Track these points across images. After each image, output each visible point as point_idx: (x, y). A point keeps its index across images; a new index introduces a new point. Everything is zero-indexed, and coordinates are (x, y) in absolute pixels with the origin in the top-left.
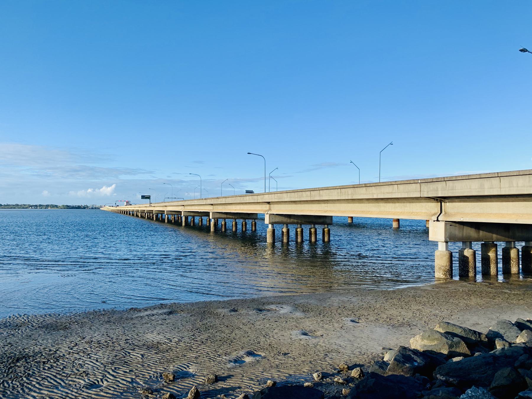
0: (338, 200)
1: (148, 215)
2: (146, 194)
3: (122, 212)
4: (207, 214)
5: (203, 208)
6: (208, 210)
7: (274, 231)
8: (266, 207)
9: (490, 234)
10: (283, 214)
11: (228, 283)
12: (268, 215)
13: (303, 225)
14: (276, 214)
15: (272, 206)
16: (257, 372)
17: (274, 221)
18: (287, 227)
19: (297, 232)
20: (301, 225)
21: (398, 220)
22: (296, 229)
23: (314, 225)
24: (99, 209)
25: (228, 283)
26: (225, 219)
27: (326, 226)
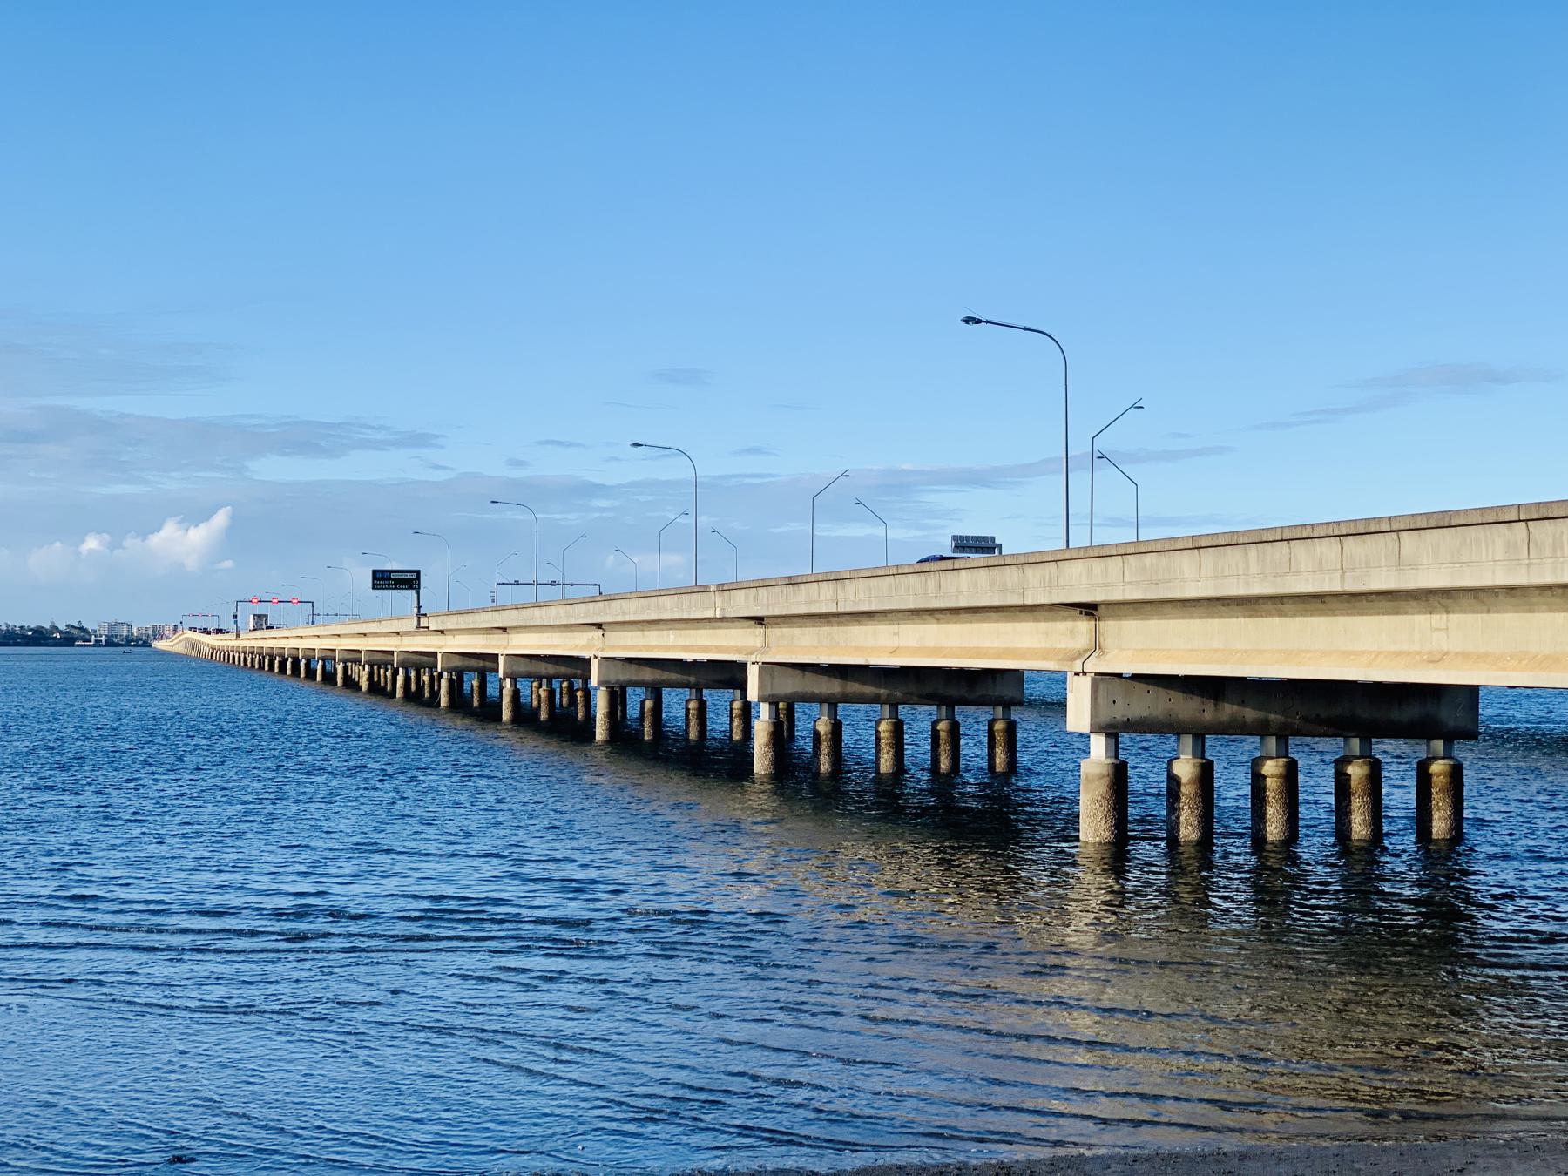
4: (730, 674)
6: (739, 650)
7: (1119, 775)
9: (685, 677)
10: (817, 665)
15: (1109, 626)
23: (1449, 741)
24: (146, 644)
27: (1438, 745)
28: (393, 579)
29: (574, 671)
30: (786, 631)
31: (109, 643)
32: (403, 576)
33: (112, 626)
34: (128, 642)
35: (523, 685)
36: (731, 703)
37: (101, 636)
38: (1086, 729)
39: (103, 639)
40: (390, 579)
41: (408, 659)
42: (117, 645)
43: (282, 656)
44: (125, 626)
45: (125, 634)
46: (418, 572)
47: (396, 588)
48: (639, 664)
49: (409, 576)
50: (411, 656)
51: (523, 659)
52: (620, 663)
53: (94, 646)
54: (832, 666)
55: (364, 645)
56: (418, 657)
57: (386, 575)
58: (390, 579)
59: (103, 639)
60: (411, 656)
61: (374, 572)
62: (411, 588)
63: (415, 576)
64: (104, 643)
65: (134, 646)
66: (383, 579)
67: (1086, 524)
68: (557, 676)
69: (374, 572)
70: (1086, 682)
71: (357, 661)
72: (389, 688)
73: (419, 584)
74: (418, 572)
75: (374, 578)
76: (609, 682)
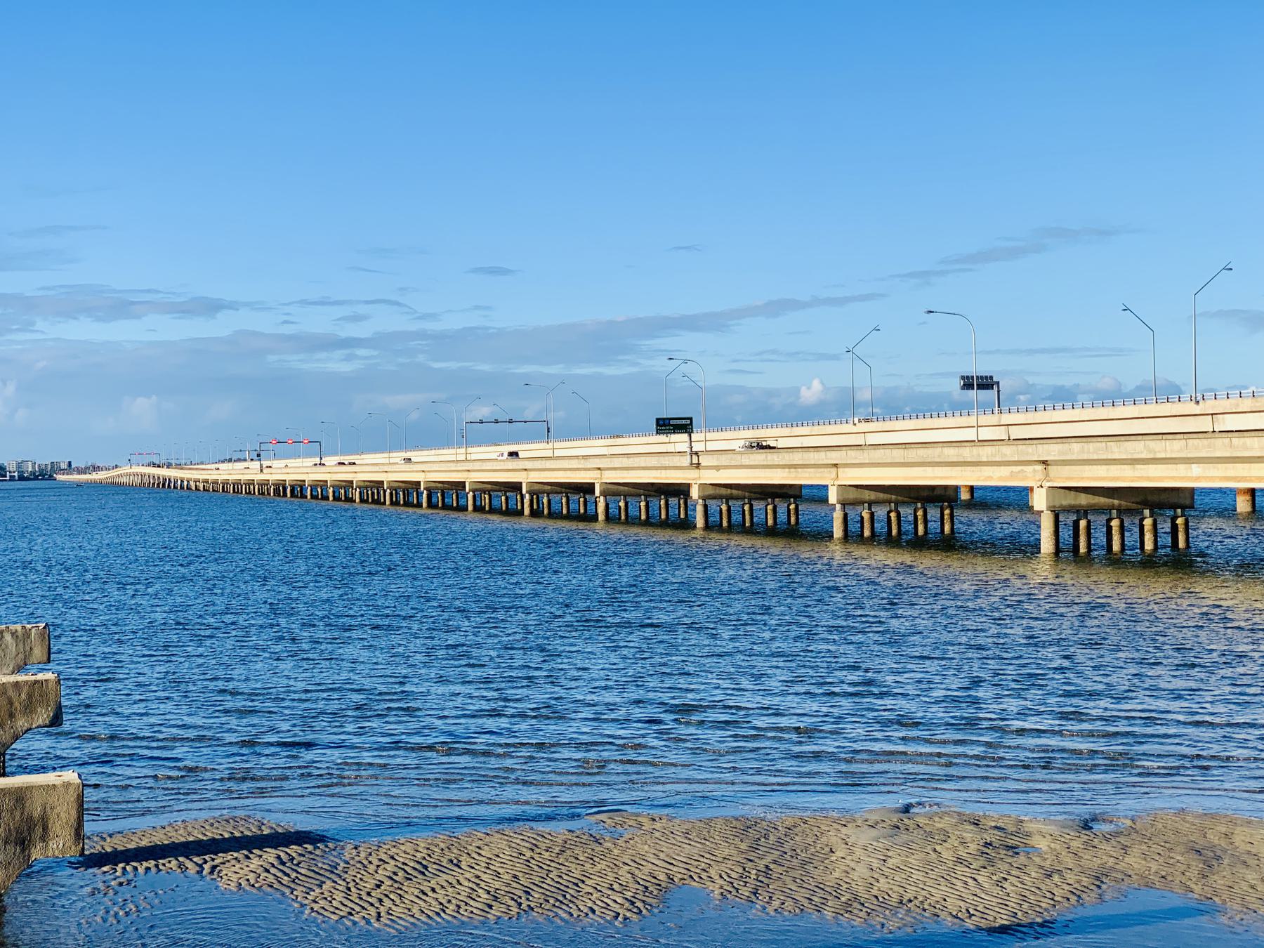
0: (1259, 457)
1: (373, 493)
2: (674, 412)
3: (285, 489)
4: (516, 487)
5: (585, 476)
6: (591, 479)
7: (845, 517)
8: (596, 474)
9: (1111, 500)
10: (863, 485)
11: (960, 790)
12: (835, 487)
13: (777, 500)
14: (1060, 488)
15: (840, 470)
16: (435, 866)
17: (707, 493)
18: (727, 503)
19: (789, 510)
20: (506, 492)
21: (1252, 492)
22: (915, 511)
23: (584, 494)
24: (51, 478)
25: (960, 790)
26: (870, 504)
27: (792, 500)
28: (672, 425)
29: (889, 496)
30: (846, 470)
31: (21, 478)
32: (679, 422)
33: (19, 464)
34: (34, 477)
35: (709, 502)
36: (766, 506)
37: (14, 472)
38: (835, 502)
39: (16, 474)
40: (670, 425)
41: (608, 489)
42: (27, 479)
43: (227, 483)
44: (30, 463)
45: (30, 469)
46: (691, 419)
47: (674, 433)
48: (1077, 491)
49: (684, 422)
50: (610, 486)
51: (851, 488)
52: (1063, 490)
53: (10, 480)
54: (867, 486)
55: (201, 477)
56: (616, 487)
57: (666, 422)
58: (670, 425)
59: (16, 474)
60: (610, 486)
61: (658, 420)
62: (686, 432)
63: (688, 422)
64: (17, 478)
65: (41, 479)
66: (664, 425)
67: (1223, 419)
68: (877, 502)
69: (658, 420)
70: (697, 486)
71: (207, 482)
72: (382, 500)
73: (692, 429)
74: (691, 419)
75: (658, 424)
76: (1054, 507)
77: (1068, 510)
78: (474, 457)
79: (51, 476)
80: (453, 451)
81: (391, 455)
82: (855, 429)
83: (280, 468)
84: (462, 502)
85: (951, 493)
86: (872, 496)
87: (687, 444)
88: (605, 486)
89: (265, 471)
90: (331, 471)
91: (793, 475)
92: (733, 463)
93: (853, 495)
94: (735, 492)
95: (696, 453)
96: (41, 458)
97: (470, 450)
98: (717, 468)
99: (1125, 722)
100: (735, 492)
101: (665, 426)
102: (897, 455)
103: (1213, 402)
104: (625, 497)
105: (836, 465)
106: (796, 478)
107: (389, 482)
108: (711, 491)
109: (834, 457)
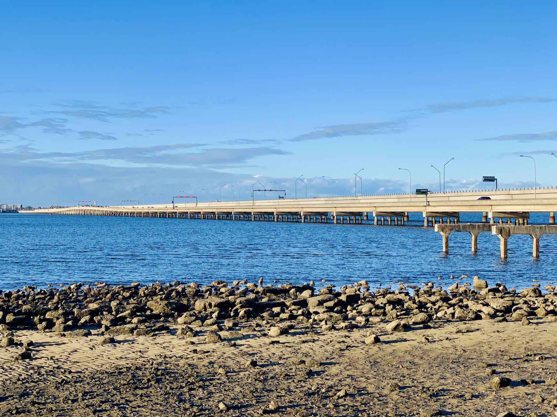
2: (422, 187)
24: (16, 211)
32: (424, 191)
49: (425, 191)
54: (511, 212)
61: (417, 190)
69: (417, 190)
75: (417, 191)
77: (429, 216)
78: (256, 204)
79: (16, 211)
80: (208, 203)
81: (240, 202)
82: (445, 195)
83: (474, 201)
84: (187, 217)
85: (361, 214)
86: (343, 214)
87: (425, 198)
88: (377, 213)
89: (175, 208)
90: (128, 208)
91: (471, 209)
92: (446, 205)
93: (497, 215)
94: (438, 215)
95: (429, 202)
96: (11, 206)
97: (255, 202)
98: (435, 206)
99: (424, 279)
100: (438, 215)
101: (419, 192)
102: (350, 205)
103: (539, 190)
104: (510, 219)
105: (491, 205)
106: (472, 210)
107: (253, 212)
108: (430, 214)
109: (448, 204)
